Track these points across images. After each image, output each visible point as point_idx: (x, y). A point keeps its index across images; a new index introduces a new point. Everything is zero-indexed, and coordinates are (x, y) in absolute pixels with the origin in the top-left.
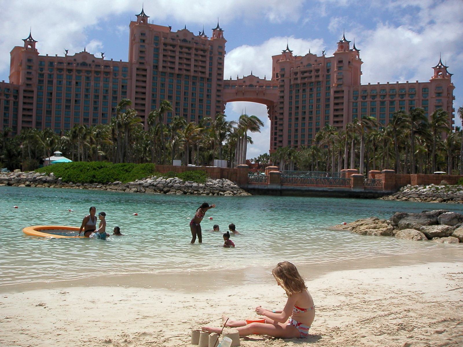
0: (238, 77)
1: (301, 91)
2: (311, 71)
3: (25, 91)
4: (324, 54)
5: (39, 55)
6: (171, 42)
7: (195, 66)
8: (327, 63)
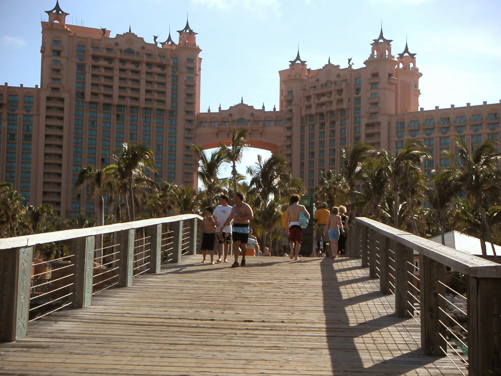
0: (220, 108)
1: (317, 126)
2: (331, 93)
3: (49, 99)
4: (351, 64)
6: (105, 53)
7: (148, 91)
8: (356, 79)
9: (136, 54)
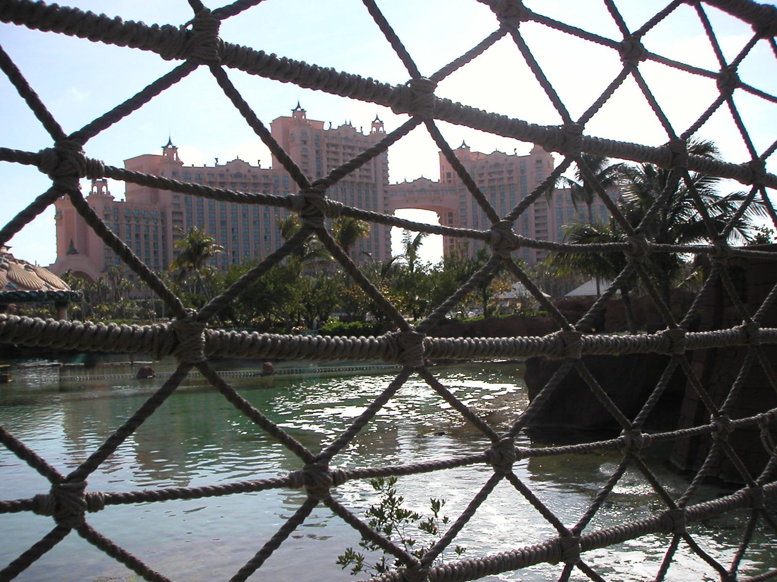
5: (114, 200)
9: (243, 176)
